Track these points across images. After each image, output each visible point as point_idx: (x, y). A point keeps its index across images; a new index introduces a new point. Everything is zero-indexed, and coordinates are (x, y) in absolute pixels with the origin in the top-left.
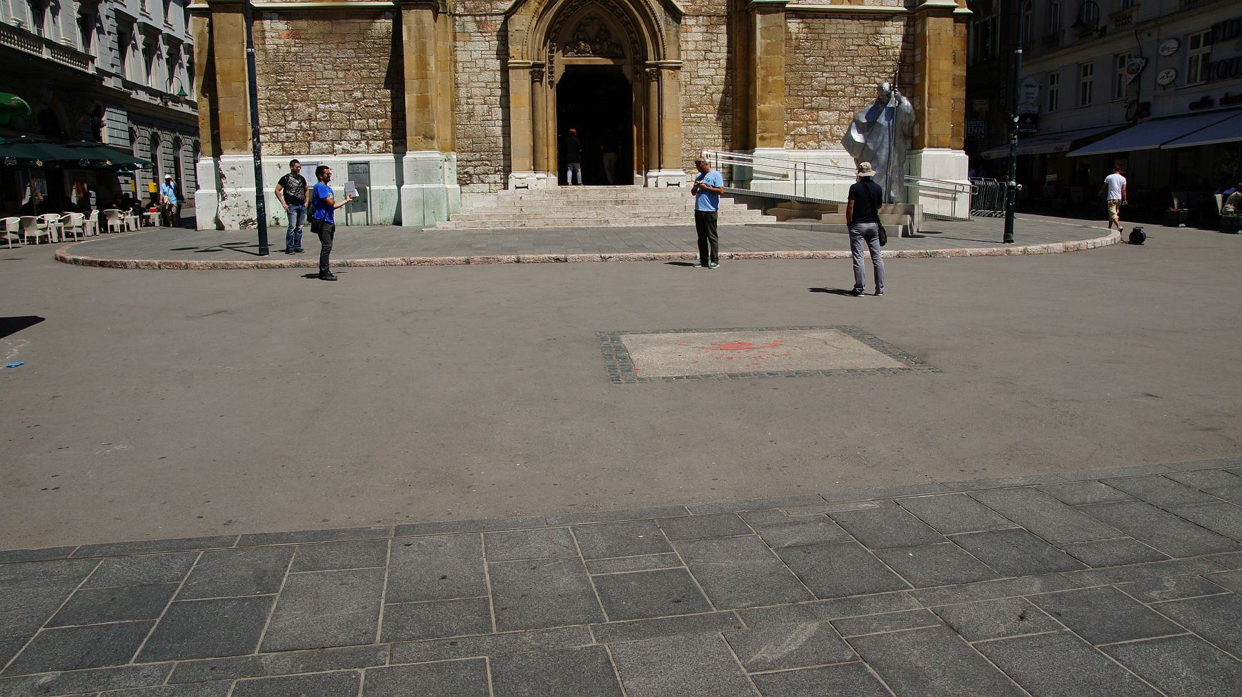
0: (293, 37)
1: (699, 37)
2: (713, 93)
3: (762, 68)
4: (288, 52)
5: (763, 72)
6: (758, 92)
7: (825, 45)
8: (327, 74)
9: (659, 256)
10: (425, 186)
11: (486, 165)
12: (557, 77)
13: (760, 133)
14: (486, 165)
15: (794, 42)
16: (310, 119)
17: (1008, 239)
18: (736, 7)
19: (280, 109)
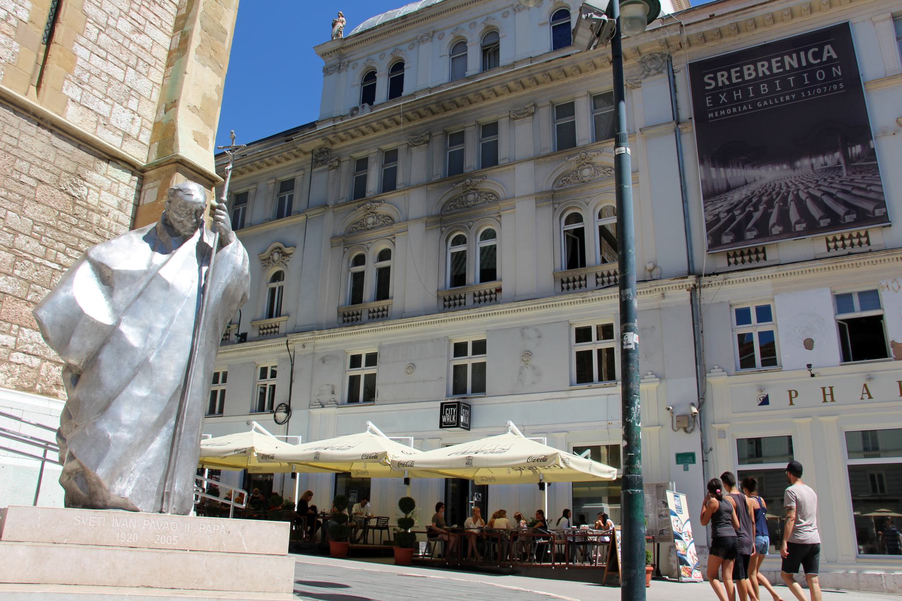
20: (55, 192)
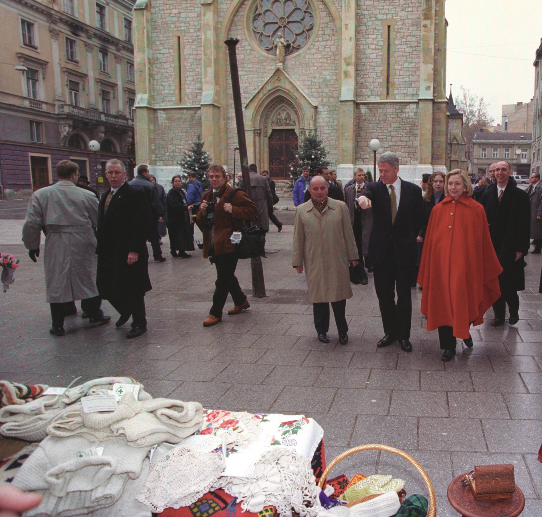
0: (168, 120)
7: (377, 118)
8: (180, 134)
16: (173, 151)
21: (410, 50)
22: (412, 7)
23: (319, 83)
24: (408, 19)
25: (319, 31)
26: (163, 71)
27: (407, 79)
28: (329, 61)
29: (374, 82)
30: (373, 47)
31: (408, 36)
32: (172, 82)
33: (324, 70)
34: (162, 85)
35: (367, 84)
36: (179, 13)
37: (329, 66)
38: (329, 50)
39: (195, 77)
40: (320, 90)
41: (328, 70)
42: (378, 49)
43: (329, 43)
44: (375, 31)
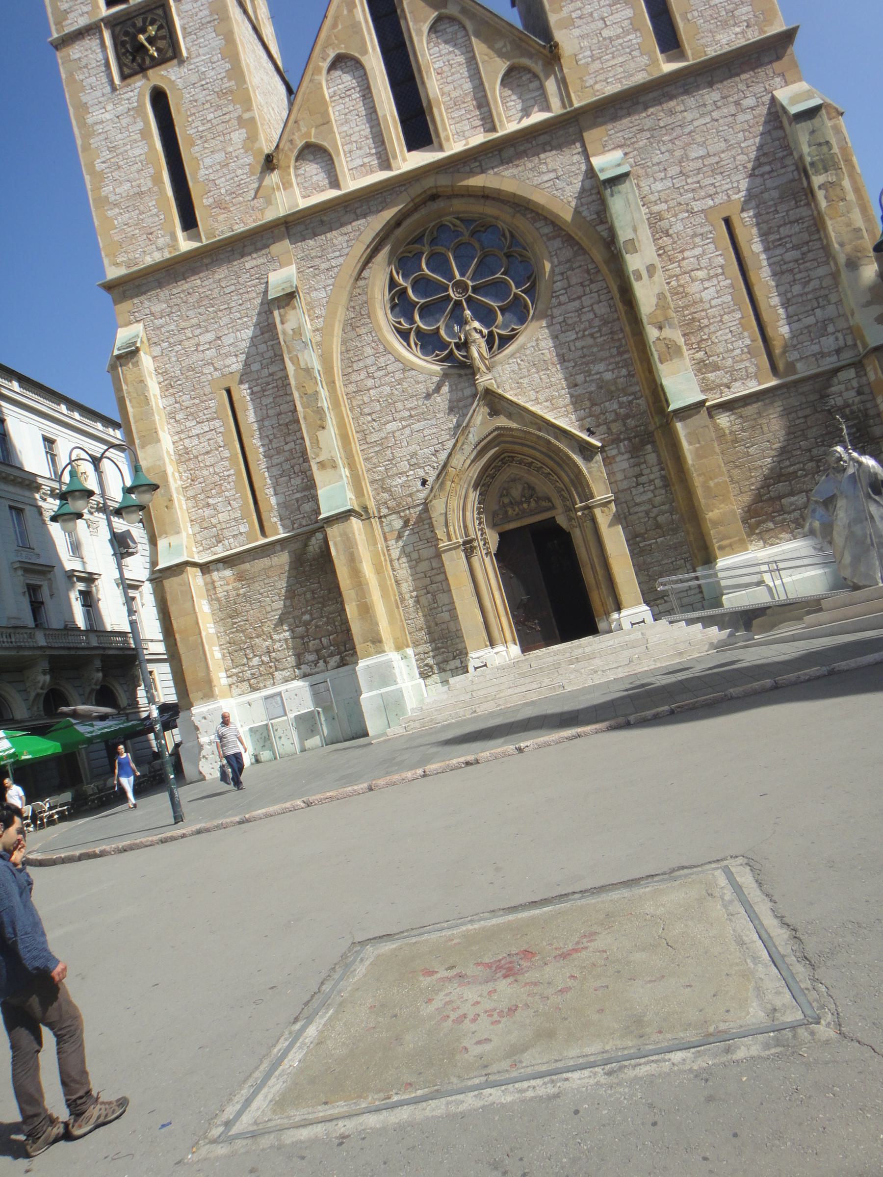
0: (239, 580)
1: (625, 465)
2: (658, 515)
3: (699, 475)
4: (238, 595)
5: (701, 479)
6: (703, 501)
7: (765, 429)
9: (584, 732)
10: (383, 690)
11: (443, 652)
12: (493, 548)
13: (717, 542)
14: (443, 652)
15: (729, 438)
17: (178, 818)
18: (655, 423)
19: (241, 649)
20: (817, 415)
21: (795, 254)
22: (770, 163)
23: (591, 393)
24: (766, 190)
25: (555, 282)
26: (206, 473)
27: (811, 320)
28: (599, 340)
29: (728, 351)
30: (701, 274)
31: (779, 227)
32: (233, 492)
33: (593, 362)
34: (208, 505)
35: (715, 358)
36: (219, 338)
37: (602, 350)
38: (591, 316)
39: (286, 466)
40: (597, 409)
41: (602, 360)
42: (717, 275)
43: (587, 301)
44: (697, 240)
